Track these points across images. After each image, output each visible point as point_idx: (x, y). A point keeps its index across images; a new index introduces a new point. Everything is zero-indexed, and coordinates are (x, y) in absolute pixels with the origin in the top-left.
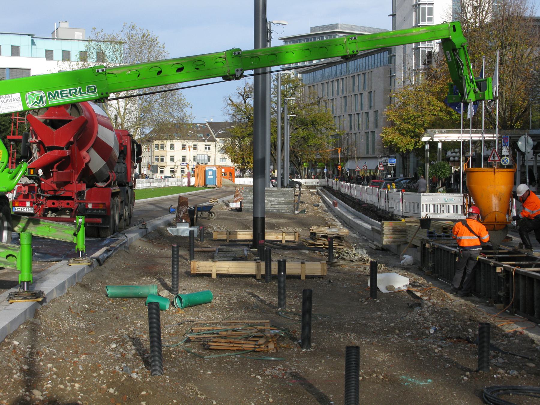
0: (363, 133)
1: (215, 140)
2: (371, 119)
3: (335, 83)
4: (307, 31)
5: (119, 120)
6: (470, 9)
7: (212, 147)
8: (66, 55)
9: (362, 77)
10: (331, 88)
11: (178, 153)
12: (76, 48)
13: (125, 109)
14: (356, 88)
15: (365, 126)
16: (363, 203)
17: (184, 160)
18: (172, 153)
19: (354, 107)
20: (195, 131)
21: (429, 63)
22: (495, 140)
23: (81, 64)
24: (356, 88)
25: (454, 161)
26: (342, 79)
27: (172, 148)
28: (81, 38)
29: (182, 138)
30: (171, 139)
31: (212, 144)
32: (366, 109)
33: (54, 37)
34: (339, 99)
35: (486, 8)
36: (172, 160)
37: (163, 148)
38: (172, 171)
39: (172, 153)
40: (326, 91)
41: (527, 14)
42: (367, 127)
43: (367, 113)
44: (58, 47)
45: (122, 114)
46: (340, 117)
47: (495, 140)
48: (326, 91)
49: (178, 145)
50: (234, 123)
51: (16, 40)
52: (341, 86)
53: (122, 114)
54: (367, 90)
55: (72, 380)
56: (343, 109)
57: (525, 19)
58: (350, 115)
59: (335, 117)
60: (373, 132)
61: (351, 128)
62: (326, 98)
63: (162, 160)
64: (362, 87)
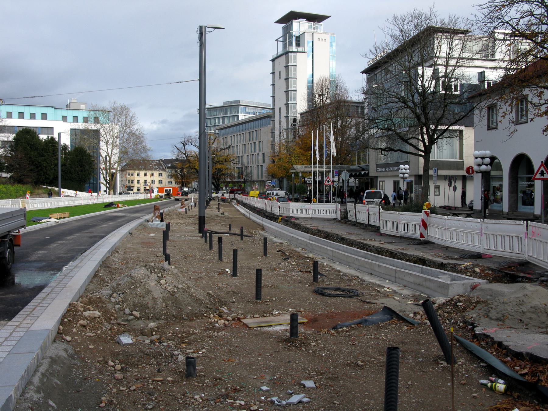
0: (256, 166)
1: (165, 170)
2: (261, 157)
3: (239, 136)
4: (222, 104)
5: (108, 158)
6: (317, 96)
7: (163, 175)
8: (75, 119)
9: (255, 133)
10: (236, 139)
11: (142, 178)
12: (81, 115)
13: (112, 152)
14: (251, 139)
15: (257, 162)
16: (257, 208)
17: (145, 182)
18: (138, 178)
19: (250, 151)
20: (153, 165)
21: (295, 125)
22: (366, 198)
23: (84, 124)
24: (251, 139)
25: (309, 183)
26: (243, 134)
27: (138, 175)
28: (84, 108)
29: (145, 169)
30: (139, 170)
31: (163, 173)
32: (257, 152)
33: (68, 107)
34: (241, 145)
35: (326, 96)
36: (138, 183)
37: (132, 175)
38: (138, 190)
39: (138, 178)
40: (233, 141)
41: (349, 99)
42: (258, 162)
43: (258, 154)
44: (70, 114)
45: (110, 154)
46: (242, 156)
47: (366, 198)
48: (233, 141)
49: (142, 173)
50: (177, 160)
51: (44, 110)
52: (242, 138)
53: (110, 154)
54: (258, 140)
55: (415, 368)
56: (244, 152)
57: (348, 102)
58: (248, 155)
59: (239, 157)
60: (262, 166)
61: (248, 163)
62: (233, 145)
63: (132, 182)
64: (255, 138)
